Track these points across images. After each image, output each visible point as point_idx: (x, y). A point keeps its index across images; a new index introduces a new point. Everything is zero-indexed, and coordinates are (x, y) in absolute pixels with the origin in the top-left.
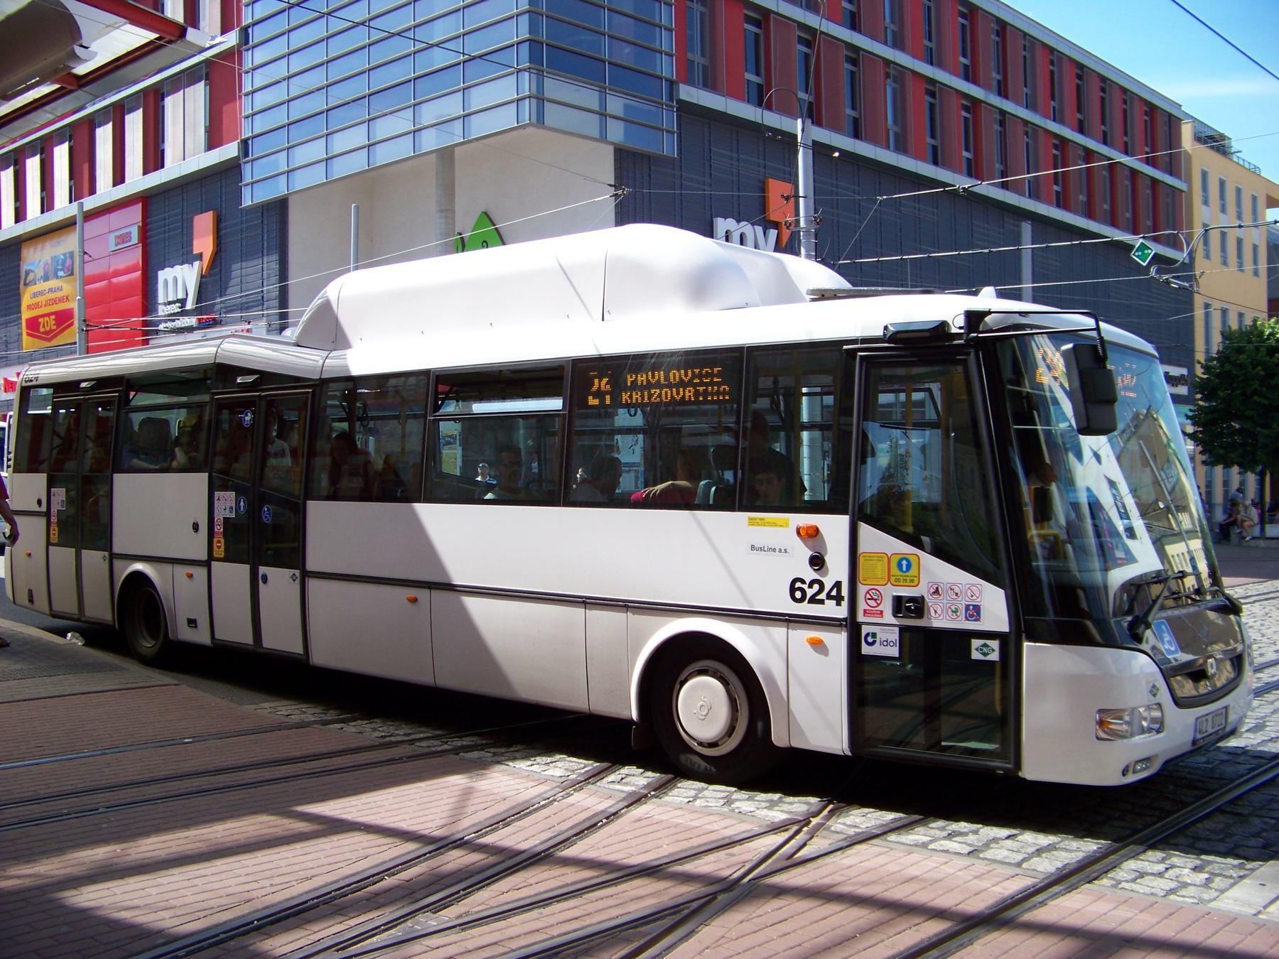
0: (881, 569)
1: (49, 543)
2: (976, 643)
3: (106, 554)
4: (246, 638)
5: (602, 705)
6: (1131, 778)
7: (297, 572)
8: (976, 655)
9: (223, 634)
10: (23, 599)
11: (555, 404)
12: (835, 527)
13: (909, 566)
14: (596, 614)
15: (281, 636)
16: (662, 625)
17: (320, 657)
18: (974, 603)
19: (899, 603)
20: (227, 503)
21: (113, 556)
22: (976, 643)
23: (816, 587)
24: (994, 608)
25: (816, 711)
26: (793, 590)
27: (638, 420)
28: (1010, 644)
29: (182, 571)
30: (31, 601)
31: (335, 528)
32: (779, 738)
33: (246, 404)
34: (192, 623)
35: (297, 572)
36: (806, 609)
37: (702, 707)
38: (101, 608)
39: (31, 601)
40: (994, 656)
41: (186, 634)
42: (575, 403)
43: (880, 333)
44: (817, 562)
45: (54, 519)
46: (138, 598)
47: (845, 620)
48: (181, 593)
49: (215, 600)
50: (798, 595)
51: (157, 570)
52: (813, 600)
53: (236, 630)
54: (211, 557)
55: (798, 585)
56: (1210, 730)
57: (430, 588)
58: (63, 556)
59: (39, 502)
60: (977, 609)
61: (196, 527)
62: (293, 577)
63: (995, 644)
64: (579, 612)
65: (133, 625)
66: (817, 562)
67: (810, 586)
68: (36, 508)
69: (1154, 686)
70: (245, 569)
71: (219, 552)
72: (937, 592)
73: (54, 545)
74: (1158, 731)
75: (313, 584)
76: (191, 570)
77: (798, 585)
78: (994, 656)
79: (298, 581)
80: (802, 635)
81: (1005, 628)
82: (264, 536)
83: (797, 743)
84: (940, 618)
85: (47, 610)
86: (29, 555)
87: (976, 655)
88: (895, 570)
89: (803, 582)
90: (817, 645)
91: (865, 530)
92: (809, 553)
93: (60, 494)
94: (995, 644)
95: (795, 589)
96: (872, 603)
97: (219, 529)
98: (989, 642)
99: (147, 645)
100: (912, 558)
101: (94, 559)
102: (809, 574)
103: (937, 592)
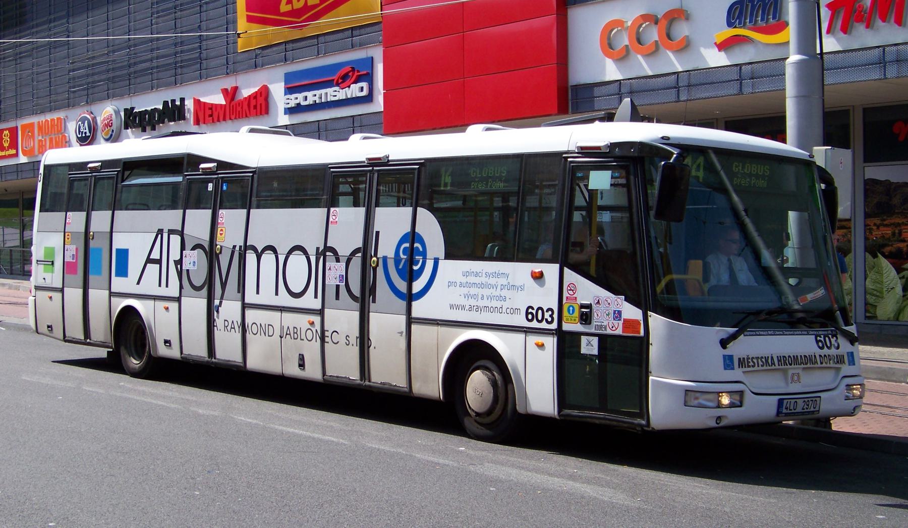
10: (43, 329)
15: (228, 349)
21: (111, 294)
22: (584, 339)
25: (540, 394)
26: (527, 313)
29: (161, 304)
36: (535, 324)
41: (162, 351)
46: (129, 327)
47: (874, 317)
48: (161, 322)
50: (530, 317)
53: (344, 366)
55: (530, 310)
57: (526, 332)
65: (128, 346)
76: (167, 304)
77: (530, 310)
83: (529, 412)
85: (62, 337)
89: (533, 309)
91: (566, 270)
99: (135, 363)
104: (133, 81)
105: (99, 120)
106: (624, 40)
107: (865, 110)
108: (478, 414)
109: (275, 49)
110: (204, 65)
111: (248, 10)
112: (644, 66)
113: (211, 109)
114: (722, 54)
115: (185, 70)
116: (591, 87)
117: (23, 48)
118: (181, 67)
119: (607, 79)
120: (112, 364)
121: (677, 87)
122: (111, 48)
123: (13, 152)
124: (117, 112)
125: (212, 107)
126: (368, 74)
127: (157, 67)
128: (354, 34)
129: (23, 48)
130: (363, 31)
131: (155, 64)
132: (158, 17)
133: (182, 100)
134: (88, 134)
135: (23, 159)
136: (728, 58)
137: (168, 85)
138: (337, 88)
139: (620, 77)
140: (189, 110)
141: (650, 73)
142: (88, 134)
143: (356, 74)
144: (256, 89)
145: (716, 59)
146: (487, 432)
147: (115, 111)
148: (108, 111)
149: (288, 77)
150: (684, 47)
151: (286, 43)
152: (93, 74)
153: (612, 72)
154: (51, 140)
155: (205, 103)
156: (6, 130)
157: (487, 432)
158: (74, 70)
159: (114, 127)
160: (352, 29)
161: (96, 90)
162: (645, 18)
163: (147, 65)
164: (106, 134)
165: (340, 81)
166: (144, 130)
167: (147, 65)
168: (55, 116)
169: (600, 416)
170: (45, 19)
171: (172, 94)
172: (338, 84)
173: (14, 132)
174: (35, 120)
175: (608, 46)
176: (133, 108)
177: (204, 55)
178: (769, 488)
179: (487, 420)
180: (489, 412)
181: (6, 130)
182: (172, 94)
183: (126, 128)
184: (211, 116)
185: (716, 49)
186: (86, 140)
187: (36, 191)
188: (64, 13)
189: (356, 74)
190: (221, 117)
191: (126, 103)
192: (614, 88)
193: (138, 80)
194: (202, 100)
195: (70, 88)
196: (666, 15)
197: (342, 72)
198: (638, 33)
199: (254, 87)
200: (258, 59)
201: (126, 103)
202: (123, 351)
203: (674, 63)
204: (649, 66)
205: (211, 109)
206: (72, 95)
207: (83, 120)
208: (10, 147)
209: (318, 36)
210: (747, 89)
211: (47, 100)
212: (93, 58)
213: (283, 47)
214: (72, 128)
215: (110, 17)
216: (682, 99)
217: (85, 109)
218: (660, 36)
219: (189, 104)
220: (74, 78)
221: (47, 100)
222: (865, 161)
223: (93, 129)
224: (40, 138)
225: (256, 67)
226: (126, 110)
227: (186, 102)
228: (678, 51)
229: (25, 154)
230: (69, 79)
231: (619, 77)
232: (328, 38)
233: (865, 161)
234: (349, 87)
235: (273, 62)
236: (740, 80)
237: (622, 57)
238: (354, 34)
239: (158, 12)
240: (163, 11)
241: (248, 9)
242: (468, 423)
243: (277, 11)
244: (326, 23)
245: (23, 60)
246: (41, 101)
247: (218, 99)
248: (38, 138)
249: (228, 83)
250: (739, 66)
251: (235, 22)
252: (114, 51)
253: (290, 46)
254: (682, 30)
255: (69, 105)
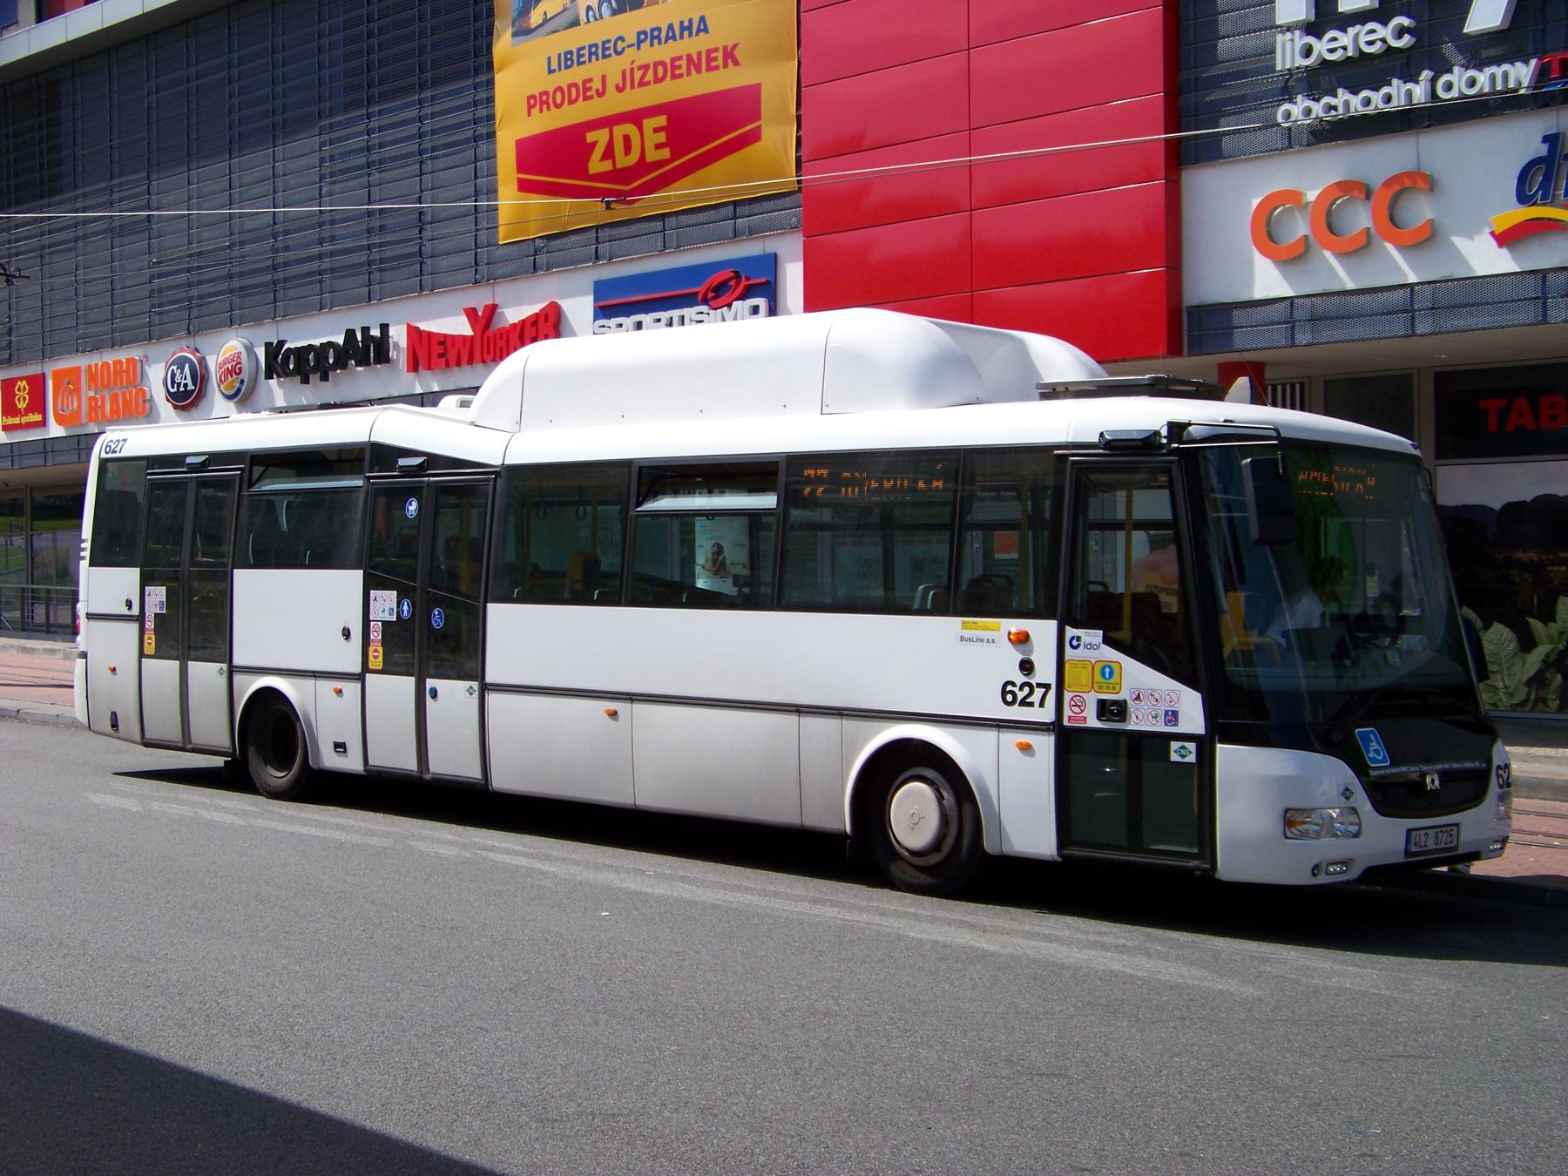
0: (1085, 677)
1: (142, 655)
2: (1174, 745)
3: (224, 666)
4: (409, 763)
5: (816, 819)
6: (1322, 879)
7: (475, 685)
8: (1174, 757)
9: (379, 759)
11: (768, 501)
12: (1043, 631)
13: (1111, 674)
14: (809, 722)
15: (453, 758)
16: (879, 731)
17: (502, 780)
18: (1166, 703)
19: (1102, 705)
20: (386, 604)
21: (232, 670)
22: (1174, 745)
23: (1027, 690)
24: (1191, 711)
25: (1026, 819)
26: (1004, 693)
27: (1012, 510)
28: (1205, 746)
29: (327, 686)
30: (115, 725)
31: (519, 634)
32: (989, 845)
33: (414, 491)
34: (340, 747)
35: (475, 685)
37: (914, 814)
38: (214, 728)
39: (115, 725)
40: (1192, 758)
41: (330, 760)
42: (790, 499)
43: (1095, 439)
44: (1026, 666)
45: (150, 625)
49: (366, 718)
50: (1009, 698)
51: (294, 685)
52: (1024, 703)
53: (396, 755)
54: (366, 669)
55: (1009, 688)
56: (1431, 846)
58: (164, 671)
59: (129, 604)
60: (1175, 714)
61: (347, 634)
62: (470, 691)
63: (1192, 746)
64: (793, 718)
65: (267, 747)
66: (1026, 666)
67: (1021, 689)
68: (125, 611)
69: (1347, 789)
70: (409, 682)
71: (376, 662)
72: (1138, 698)
73: (149, 657)
74: (1357, 835)
75: (493, 699)
77: (1009, 688)
78: (1192, 758)
79: (476, 695)
80: (1012, 738)
81: (1201, 731)
82: (436, 640)
83: (1007, 850)
84: (1140, 721)
85: (138, 737)
86: (114, 670)
87: (1174, 757)
88: (1098, 678)
89: (1013, 684)
90: (1026, 748)
92: (1020, 657)
93: (157, 596)
94: (1192, 746)
95: (1007, 693)
96: (1076, 709)
97: (376, 635)
98: (1187, 745)
99: (277, 777)
100: (1114, 666)
101: (206, 674)
102: (1019, 678)
103: (1138, 698)
104: (281, 294)
105: (212, 363)
106: (1300, 227)
107: (1438, 376)
108: (914, 853)
109: (574, 238)
110: (428, 267)
111: (519, 171)
112: (1340, 275)
113: (441, 343)
114: (1504, 251)
115: (388, 275)
116: (1227, 309)
117: (91, 227)
118: (381, 270)
119: (1258, 294)
120: (232, 777)
121: (1409, 311)
122: (236, 238)
123: (38, 417)
124: (250, 350)
125: (444, 340)
126: (767, 282)
127: (332, 270)
128: (739, 212)
129: (91, 227)
130: (756, 207)
131: (327, 263)
132: (333, 183)
133: (384, 328)
134: (191, 387)
135: (55, 430)
136: (1515, 259)
137: (350, 302)
138: (704, 308)
139: (1290, 293)
140: (396, 345)
141: (1350, 286)
142: (191, 387)
143: (744, 283)
144: (537, 308)
145: (1485, 258)
146: (923, 879)
147: (246, 347)
148: (227, 347)
149: (600, 289)
150: (1425, 239)
151: (597, 228)
152: (200, 283)
153: (1267, 280)
154: (114, 398)
155: (430, 334)
156: (21, 379)
157: (923, 879)
158: (160, 276)
159: (245, 375)
160: (735, 203)
161: (205, 310)
162: (1345, 187)
163: (314, 266)
164: (228, 388)
165: (711, 295)
166: (305, 381)
167: (314, 266)
168: (123, 355)
169: (1124, 849)
170: (104, 185)
171: (366, 319)
172: (705, 301)
173: (37, 383)
174: (81, 362)
175: (1266, 234)
176: (281, 343)
177: (428, 248)
178: (1364, 956)
179: (934, 859)
180: (936, 845)
181: (21, 379)
182: (366, 319)
183: (269, 376)
184: (441, 356)
185: (1493, 243)
186: (187, 399)
187: (85, 485)
188: (144, 174)
189: (744, 283)
190: (465, 358)
191: (270, 333)
192: (1278, 311)
193: (291, 293)
194: (424, 326)
195: (152, 306)
196: (1387, 184)
197: (716, 278)
198: (1329, 213)
199: (531, 302)
200: (539, 256)
201: (270, 333)
202: (252, 752)
203: (1401, 267)
204: (1349, 273)
205: (441, 343)
206: (156, 319)
207: (181, 363)
208: (28, 410)
209: (663, 217)
210: (1302, 338)
211: (107, 327)
212: (200, 254)
213: (593, 234)
214: (156, 377)
215: (236, 183)
216: (1418, 332)
217: (184, 344)
218: (1314, 228)
219: (398, 335)
220: (160, 291)
221: (107, 327)
222: (1438, 457)
223: (201, 377)
224: (92, 394)
225: (535, 269)
226: (268, 345)
227: (392, 331)
228: (1408, 247)
229: (60, 420)
230: (152, 291)
231: (1286, 291)
232: (684, 219)
233: (1438, 457)
234: (729, 305)
235: (571, 263)
236: (1543, 299)
237: (1292, 258)
238: (739, 212)
239: (332, 175)
240: (446, 146)
241: (522, 166)
242: (896, 870)
243: (585, 176)
244: (677, 194)
245: (56, 257)
246: (94, 329)
247: (459, 326)
248: (88, 393)
249: (479, 299)
250: (1543, 274)
251: (492, 192)
252: (242, 243)
253: (604, 234)
254: (1420, 210)
255: (151, 334)
